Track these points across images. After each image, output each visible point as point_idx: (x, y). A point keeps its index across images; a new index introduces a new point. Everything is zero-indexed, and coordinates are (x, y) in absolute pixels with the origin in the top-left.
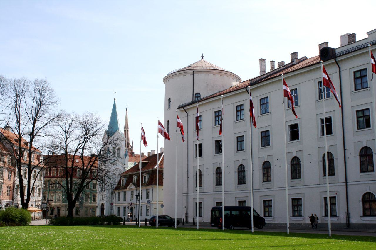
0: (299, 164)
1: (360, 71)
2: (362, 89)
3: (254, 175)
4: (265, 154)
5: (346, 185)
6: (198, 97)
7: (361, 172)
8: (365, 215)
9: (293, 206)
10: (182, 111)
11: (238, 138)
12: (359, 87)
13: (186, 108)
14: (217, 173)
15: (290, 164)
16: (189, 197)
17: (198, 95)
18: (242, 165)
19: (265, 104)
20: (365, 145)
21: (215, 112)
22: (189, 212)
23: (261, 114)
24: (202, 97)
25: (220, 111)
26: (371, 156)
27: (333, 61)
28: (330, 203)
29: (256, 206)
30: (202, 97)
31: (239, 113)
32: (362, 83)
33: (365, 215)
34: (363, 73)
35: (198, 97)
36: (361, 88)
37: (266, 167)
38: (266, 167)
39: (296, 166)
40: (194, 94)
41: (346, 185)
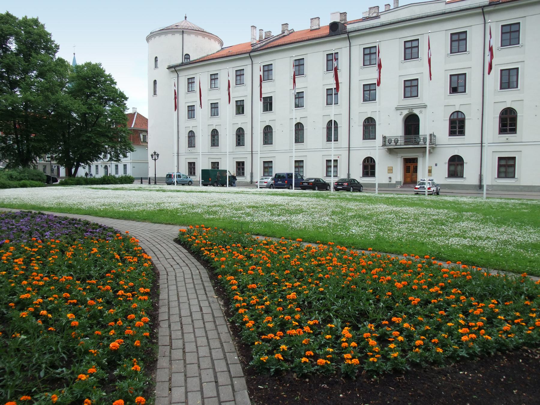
0: (271, 132)
1: (370, 48)
2: (370, 65)
3: (227, 138)
4: (267, 118)
5: (349, 150)
6: (187, 58)
7: (364, 139)
8: (499, 177)
9: (265, 168)
10: (172, 71)
11: (503, 72)
12: (238, 82)
13: (177, 69)
14: (189, 137)
15: (262, 131)
16: (485, 149)
17: (187, 56)
18: (191, 131)
19: (268, 71)
20: (509, 106)
21: (188, 79)
22: (484, 173)
23: (502, 46)
24: (192, 59)
25: (376, 47)
26: (302, 129)
27: (346, 36)
28: (331, 165)
29: (228, 166)
30: (191, 59)
31: (213, 82)
32: (510, 39)
33: (499, 177)
34: (301, 63)
35: (187, 58)
36: (369, 64)
37: (215, 134)
38: (215, 134)
39: (240, 135)
40: (184, 55)
41: (349, 150)
